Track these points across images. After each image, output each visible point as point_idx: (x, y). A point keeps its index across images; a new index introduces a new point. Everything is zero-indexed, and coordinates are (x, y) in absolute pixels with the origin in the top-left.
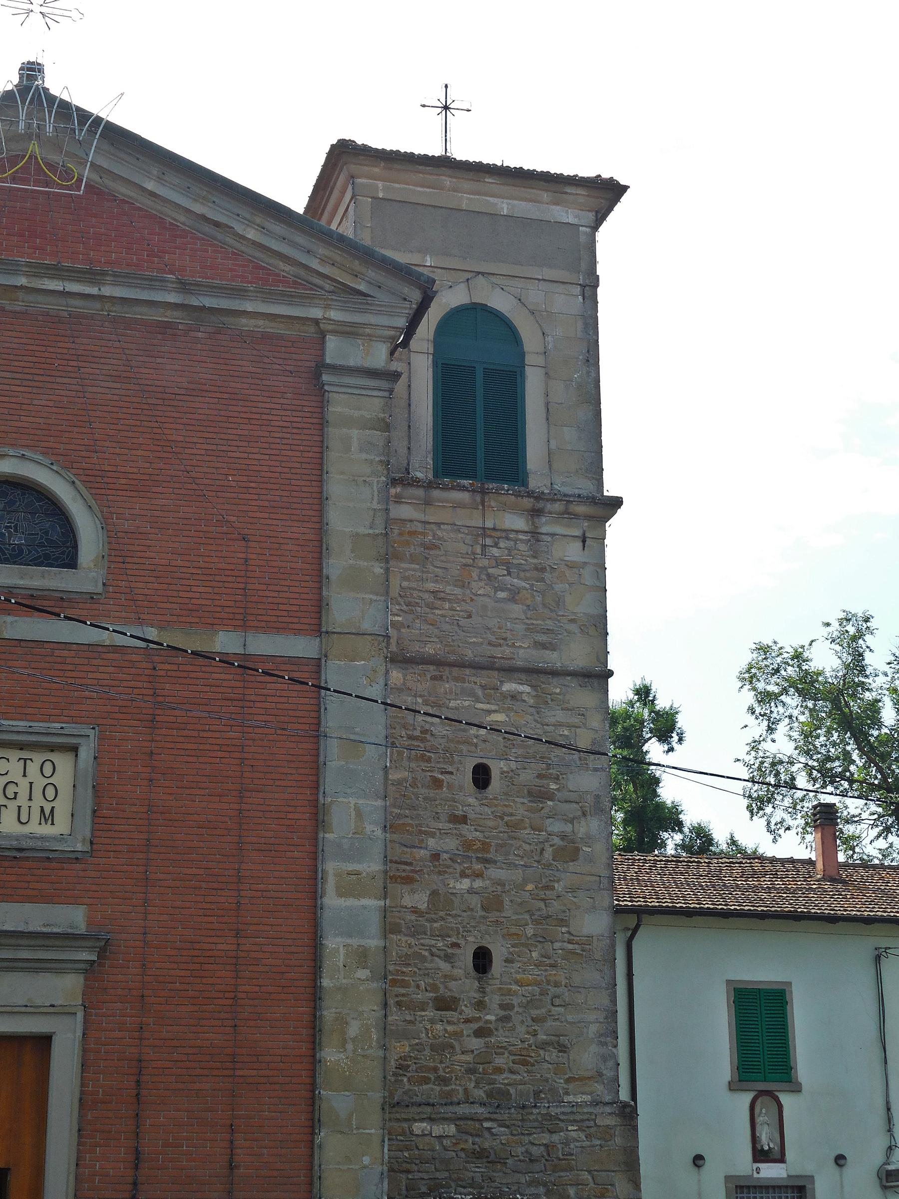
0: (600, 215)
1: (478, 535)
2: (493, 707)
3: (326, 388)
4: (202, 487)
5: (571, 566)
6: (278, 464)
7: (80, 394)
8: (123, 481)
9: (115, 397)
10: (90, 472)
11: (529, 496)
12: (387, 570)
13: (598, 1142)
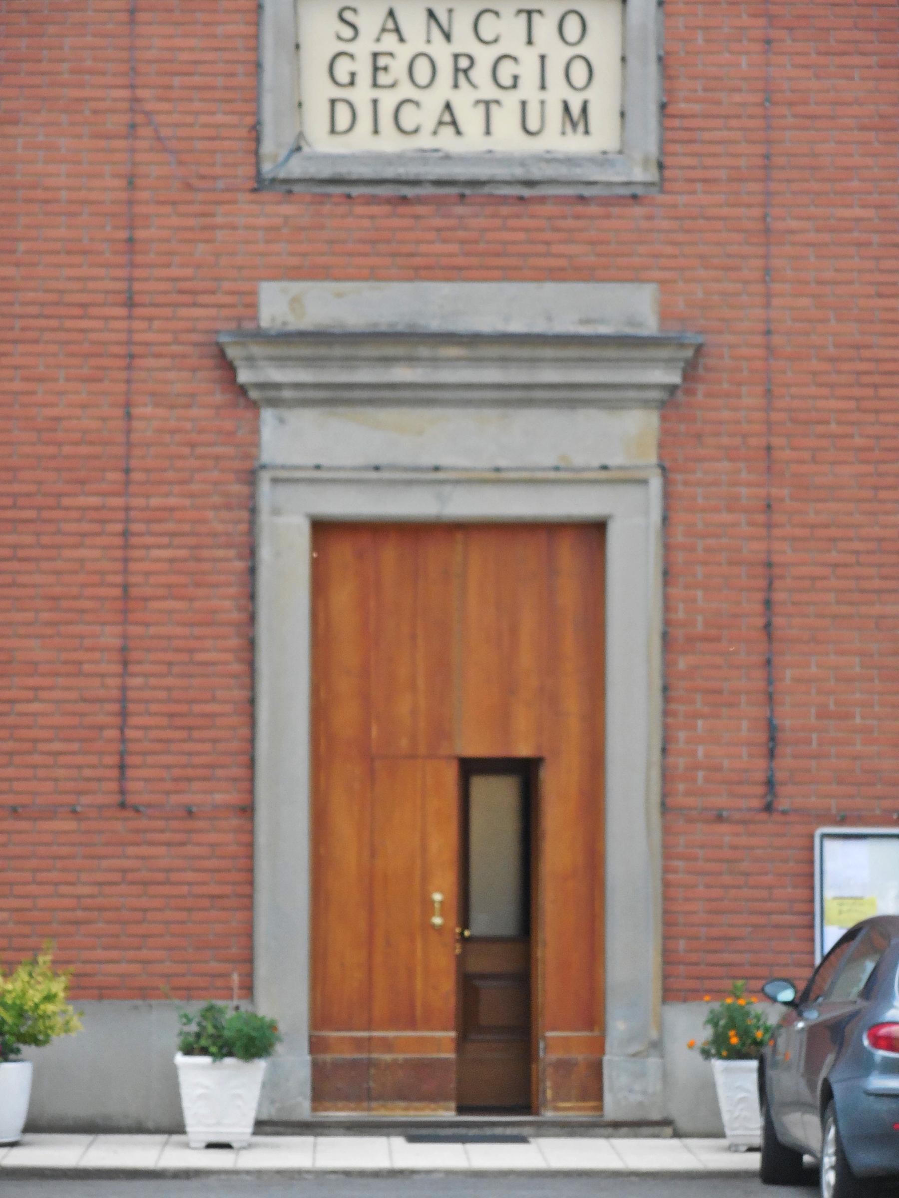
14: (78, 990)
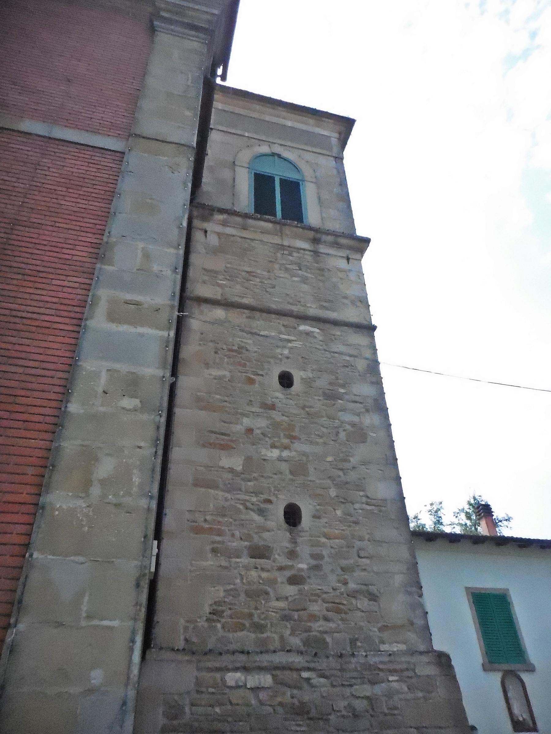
2: (293, 338)
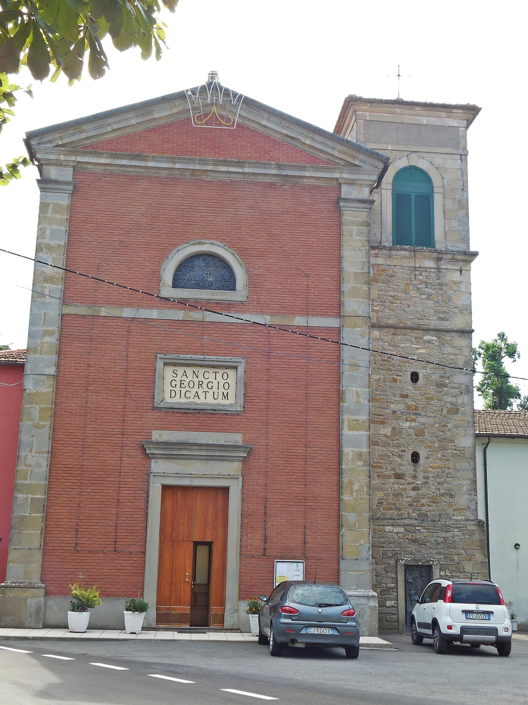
0: (469, 122)
1: (412, 270)
2: (420, 347)
3: (342, 208)
4: (288, 254)
5: (455, 283)
6: (321, 243)
7: (236, 216)
8: (255, 252)
9: (251, 216)
10: (241, 249)
11: (436, 252)
12: (369, 288)
13: (468, 537)
14: (102, 595)
